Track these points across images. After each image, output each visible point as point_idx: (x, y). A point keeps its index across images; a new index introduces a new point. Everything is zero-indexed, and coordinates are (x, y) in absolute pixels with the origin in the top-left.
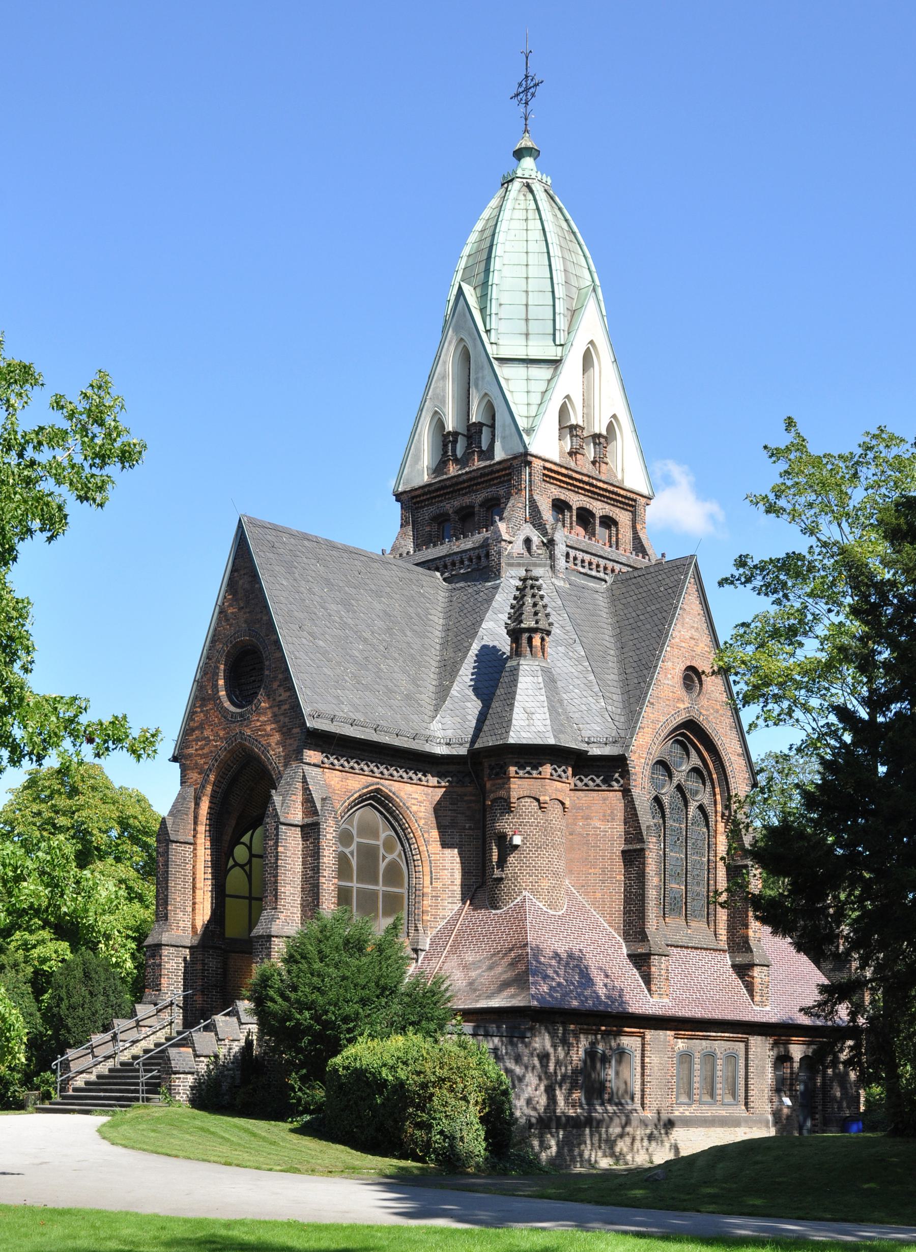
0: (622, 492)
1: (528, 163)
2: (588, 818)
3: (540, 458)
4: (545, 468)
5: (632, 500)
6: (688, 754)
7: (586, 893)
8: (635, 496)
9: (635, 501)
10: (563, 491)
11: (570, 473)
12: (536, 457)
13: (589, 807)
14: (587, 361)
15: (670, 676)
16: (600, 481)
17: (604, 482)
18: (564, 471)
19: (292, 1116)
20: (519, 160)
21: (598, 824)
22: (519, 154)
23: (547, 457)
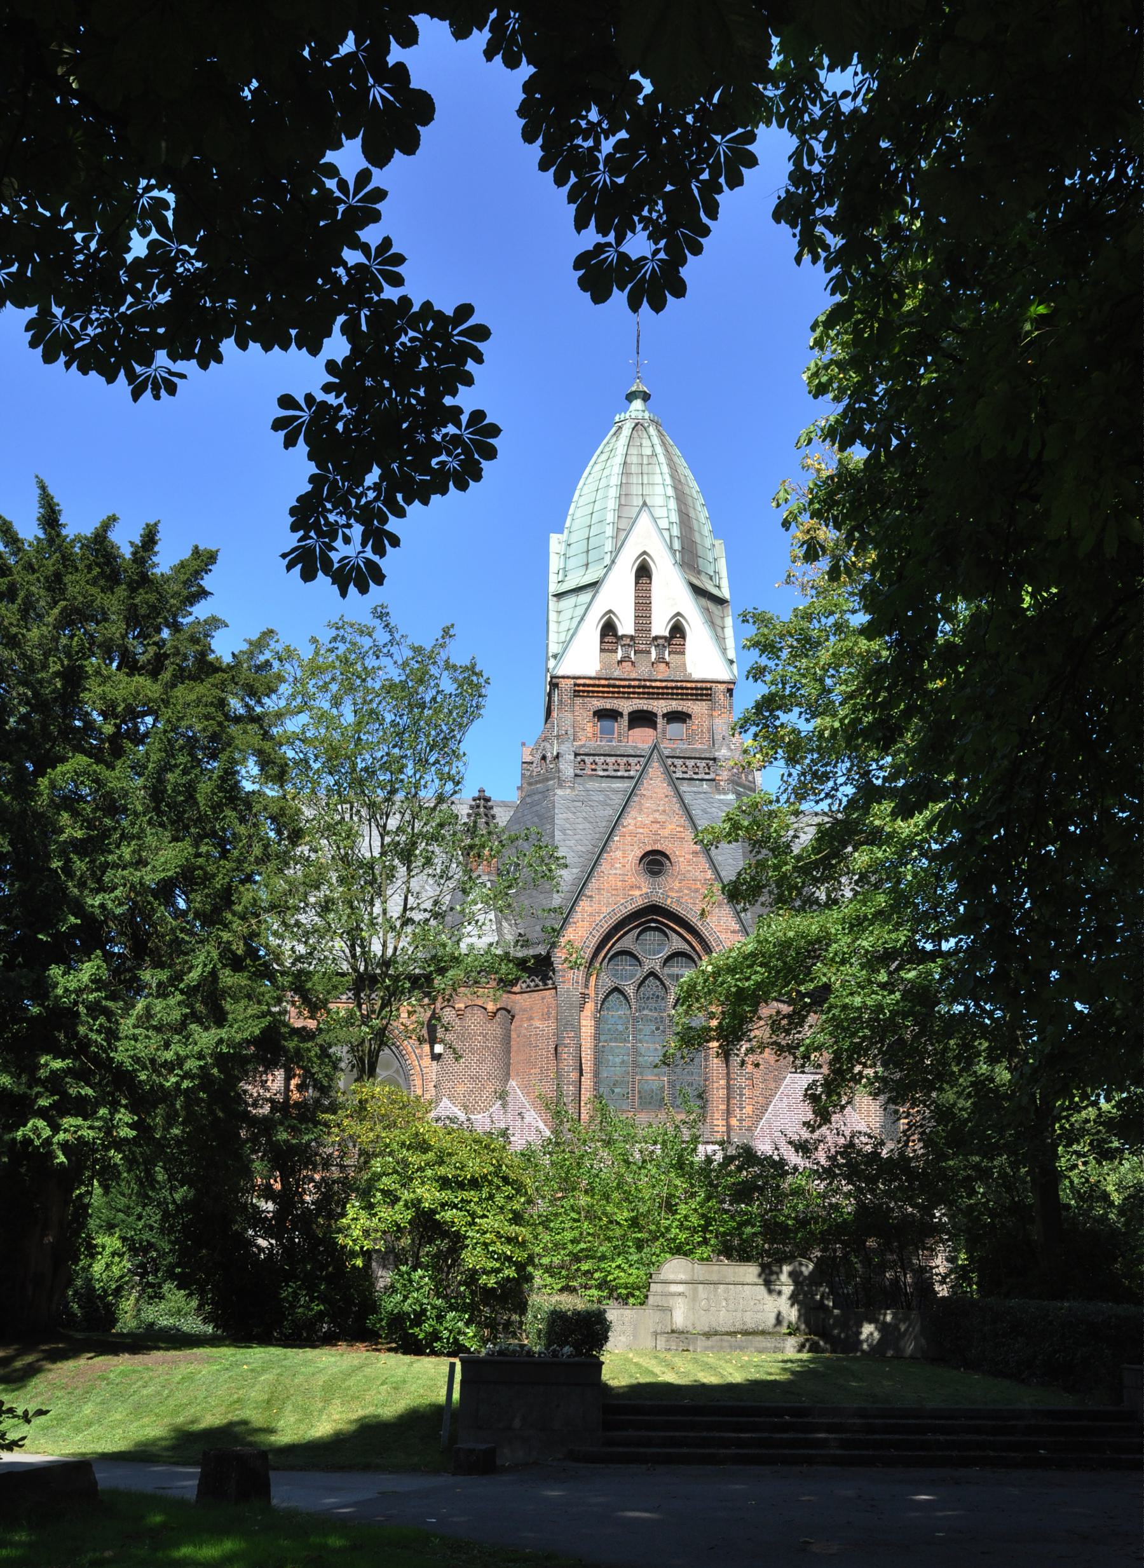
0: (689, 685)
1: (638, 404)
2: (531, 1018)
3: (568, 677)
4: (576, 685)
5: (707, 689)
6: (666, 935)
7: (528, 1094)
8: (708, 685)
9: (711, 689)
10: (609, 700)
11: (612, 682)
12: (563, 677)
13: (531, 1009)
14: (643, 572)
15: (618, 865)
16: (656, 681)
17: (661, 681)
18: (603, 682)
19: (370, 1341)
20: (631, 402)
21: (537, 1023)
22: (631, 397)
23: (578, 673)
